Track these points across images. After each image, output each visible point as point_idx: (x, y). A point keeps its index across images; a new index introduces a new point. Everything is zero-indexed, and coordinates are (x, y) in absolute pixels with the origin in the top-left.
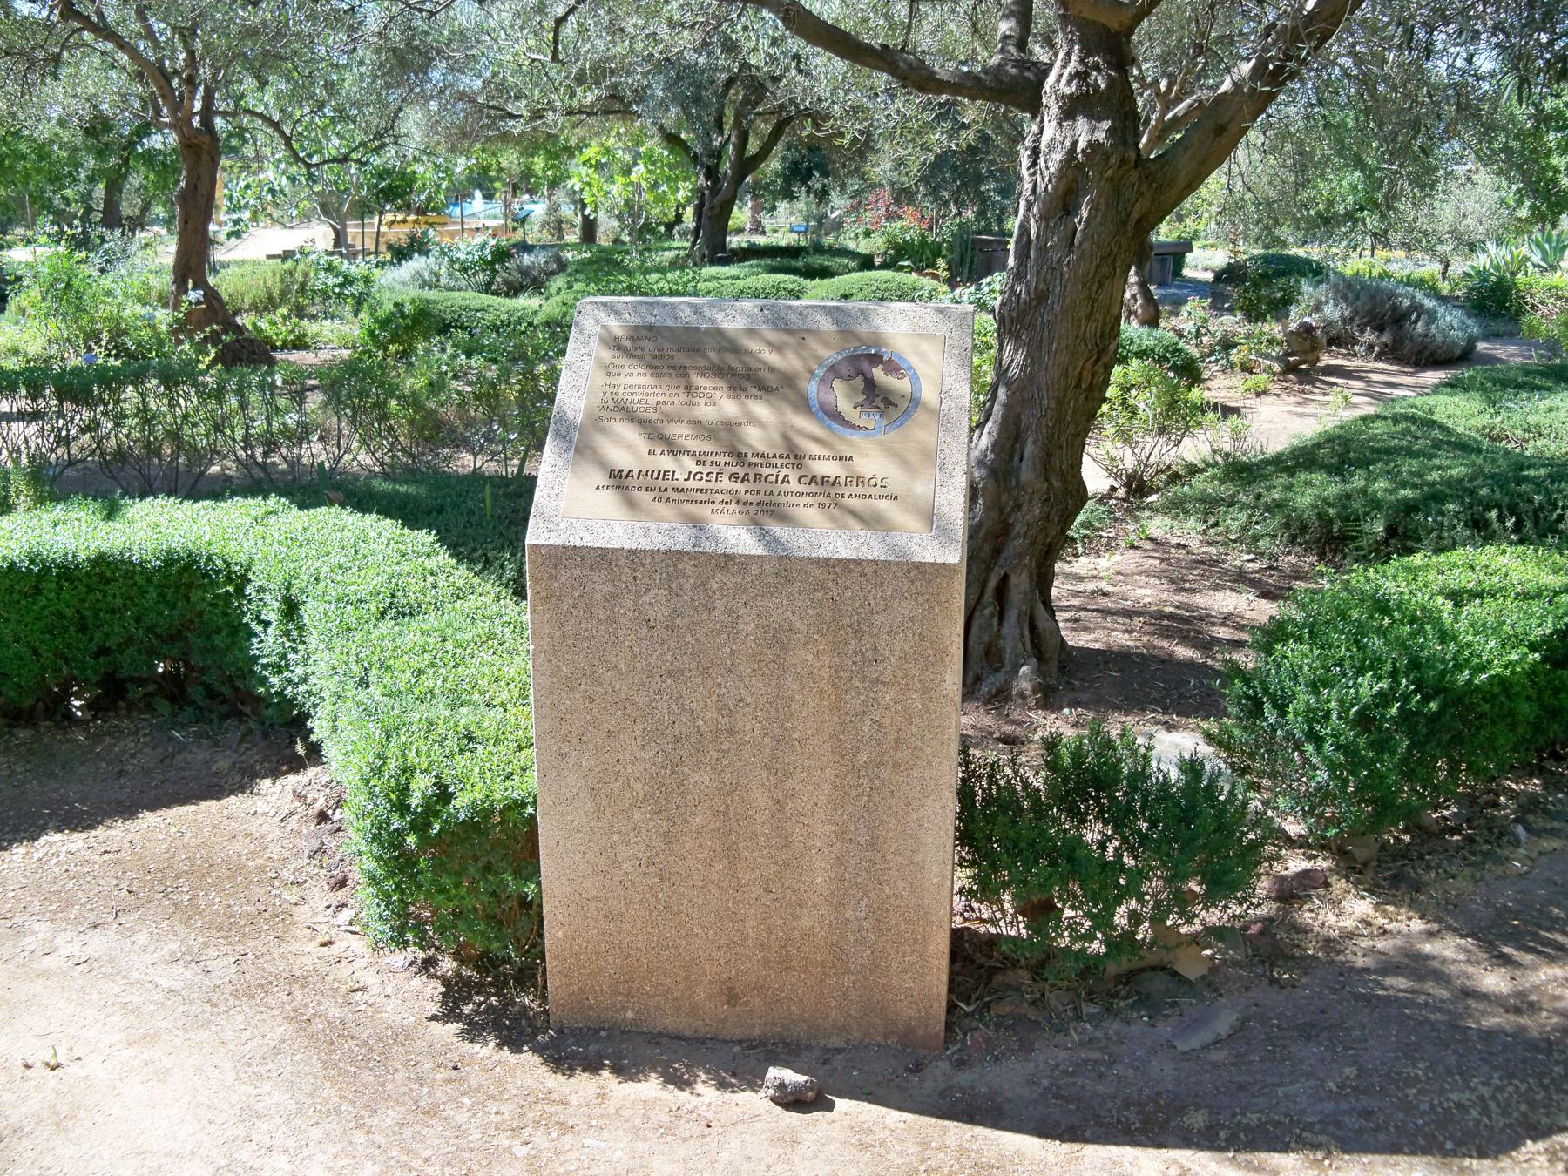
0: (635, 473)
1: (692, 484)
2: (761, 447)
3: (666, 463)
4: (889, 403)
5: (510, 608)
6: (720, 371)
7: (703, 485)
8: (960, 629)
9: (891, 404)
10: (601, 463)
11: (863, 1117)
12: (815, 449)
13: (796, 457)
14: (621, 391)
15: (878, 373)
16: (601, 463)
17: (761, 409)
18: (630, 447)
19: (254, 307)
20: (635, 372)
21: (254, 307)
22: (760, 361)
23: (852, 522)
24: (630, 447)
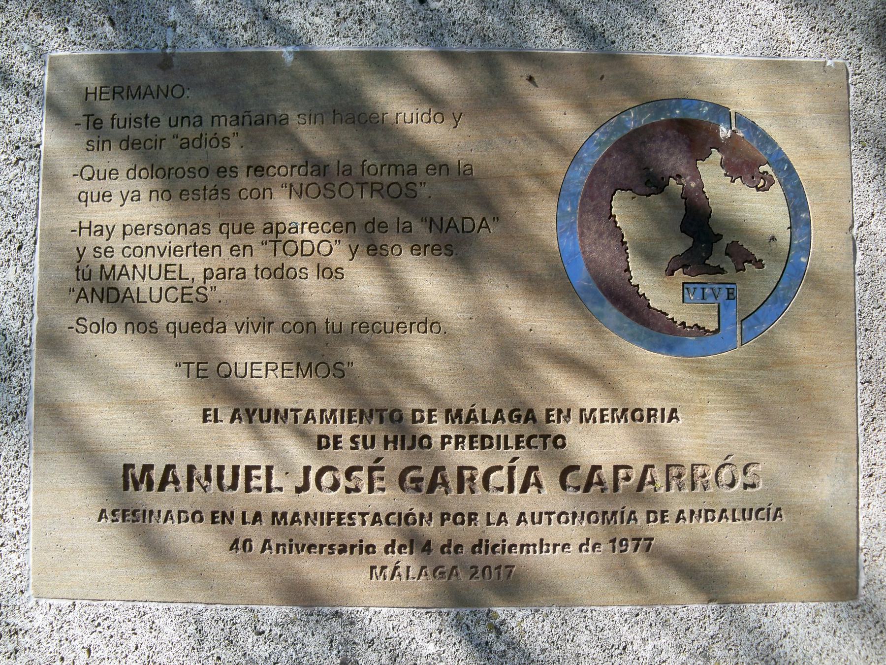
0: (181, 473)
1: (319, 500)
2: (455, 394)
3: (238, 447)
4: (742, 257)
5: (737, 110)
6: (321, 180)
7: (336, 501)
8: (860, 526)
9: (750, 258)
10: (83, 450)
11: (767, 122)
12: (582, 395)
13: (536, 429)
14: (117, 243)
15: (714, 180)
16: (83, 450)
17: (430, 284)
18: (148, 409)
19: (812, 82)
20: (118, 186)
21: (812, 82)
22: (413, 145)
23: (677, 587)
24: (148, 409)
